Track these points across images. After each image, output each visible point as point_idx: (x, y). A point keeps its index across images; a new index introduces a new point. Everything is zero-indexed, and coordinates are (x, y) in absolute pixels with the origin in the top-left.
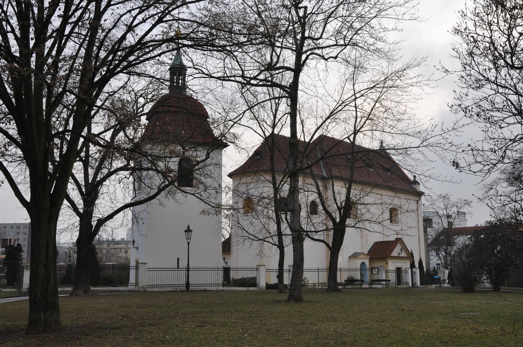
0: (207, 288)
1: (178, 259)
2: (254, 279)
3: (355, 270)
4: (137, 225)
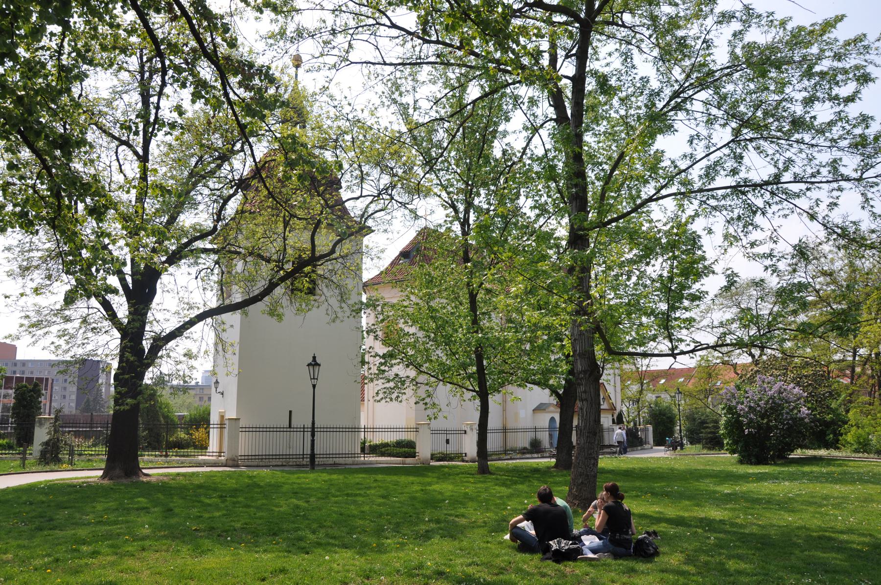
0: (337, 460)
1: (290, 412)
2: (411, 445)
3: (542, 429)
4: (224, 356)
